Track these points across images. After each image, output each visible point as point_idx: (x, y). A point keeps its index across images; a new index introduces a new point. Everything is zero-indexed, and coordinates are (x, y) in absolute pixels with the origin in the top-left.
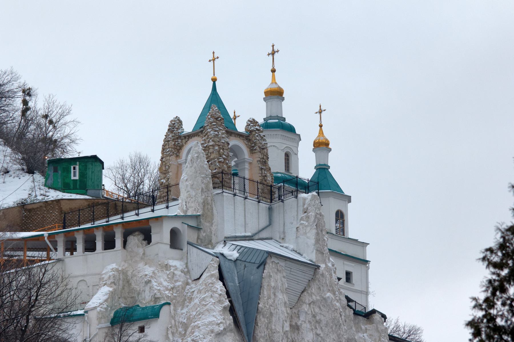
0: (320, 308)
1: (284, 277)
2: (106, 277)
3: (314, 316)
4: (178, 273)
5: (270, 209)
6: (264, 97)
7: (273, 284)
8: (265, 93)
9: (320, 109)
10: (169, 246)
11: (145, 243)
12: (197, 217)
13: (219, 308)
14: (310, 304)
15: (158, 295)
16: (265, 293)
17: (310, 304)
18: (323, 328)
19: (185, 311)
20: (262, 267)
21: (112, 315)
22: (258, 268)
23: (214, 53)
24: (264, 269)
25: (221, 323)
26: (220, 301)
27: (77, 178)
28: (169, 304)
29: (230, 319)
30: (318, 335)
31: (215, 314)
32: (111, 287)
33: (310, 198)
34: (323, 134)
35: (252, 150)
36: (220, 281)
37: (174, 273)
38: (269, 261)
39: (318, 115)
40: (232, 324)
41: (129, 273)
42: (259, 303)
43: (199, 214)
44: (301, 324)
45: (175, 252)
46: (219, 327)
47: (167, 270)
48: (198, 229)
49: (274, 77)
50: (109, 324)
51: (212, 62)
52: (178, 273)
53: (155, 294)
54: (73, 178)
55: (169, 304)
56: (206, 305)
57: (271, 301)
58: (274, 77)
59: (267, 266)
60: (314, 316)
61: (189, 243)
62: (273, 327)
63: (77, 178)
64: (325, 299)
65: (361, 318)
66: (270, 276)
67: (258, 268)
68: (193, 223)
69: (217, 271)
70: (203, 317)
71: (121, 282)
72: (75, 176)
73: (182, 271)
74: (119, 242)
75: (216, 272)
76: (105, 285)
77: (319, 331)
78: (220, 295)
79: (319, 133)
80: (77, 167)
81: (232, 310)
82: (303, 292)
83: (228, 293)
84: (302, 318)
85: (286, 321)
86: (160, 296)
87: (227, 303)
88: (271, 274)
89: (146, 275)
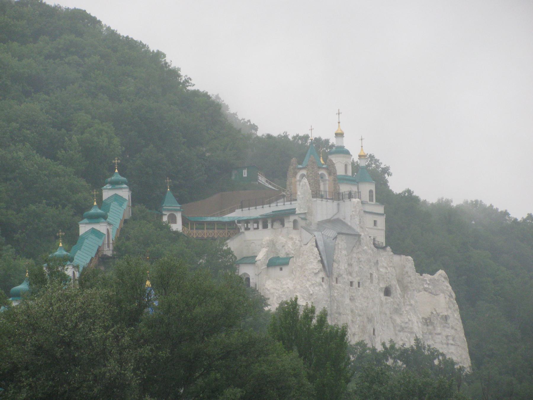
0: (361, 254)
1: (345, 243)
2: (264, 243)
3: (359, 259)
4: (297, 242)
5: (338, 204)
6: (335, 136)
7: (340, 247)
8: (335, 134)
9: (362, 138)
10: (292, 228)
11: (281, 226)
12: (305, 213)
13: (316, 261)
14: (357, 253)
15: (288, 253)
16: (337, 252)
17: (357, 253)
18: (363, 264)
19: (300, 260)
20: (335, 240)
21: (267, 262)
22: (333, 240)
23: (311, 126)
24: (336, 240)
25: (317, 268)
26: (316, 258)
27: (246, 176)
28: (293, 257)
29: (320, 266)
30: (360, 267)
31: (314, 264)
32: (267, 248)
33: (356, 202)
34: (363, 150)
35: (330, 174)
36: (316, 248)
37: (295, 242)
38: (338, 237)
39: (361, 141)
40: (322, 268)
41: (275, 241)
42: (334, 257)
43: (306, 212)
44: (353, 263)
45: (295, 231)
46: (316, 270)
47: (292, 240)
48: (305, 219)
49: (339, 126)
50: (266, 267)
51: (310, 130)
52: (297, 242)
53: (287, 252)
54: (244, 176)
55: (293, 257)
56: (310, 259)
57: (339, 255)
58: (339, 126)
59: (337, 239)
60: (359, 259)
61: (302, 227)
62: (340, 267)
63: (246, 176)
64: (363, 250)
65: (381, 250)
66: (339, 244)
67: (333, 240)
68: (303, 216)
69: (315, 243)
70: (309, 265)
71: (271, 245)
72: (245, 175)
73: (299, 241)
74: (269, 225)
75: (314, 244)
76: (263, 247)
77: (361, 266)
78: (316, 255)
79: (361, 150)
80: (246, 171)
81: (322, 261)
82: (354, 247)
83: (320, 254)
84: (353, 261)
85: (346, 263)
86: (289, 253)
87: (319, 258)
88: (339, 243)
89: (282, 243)
